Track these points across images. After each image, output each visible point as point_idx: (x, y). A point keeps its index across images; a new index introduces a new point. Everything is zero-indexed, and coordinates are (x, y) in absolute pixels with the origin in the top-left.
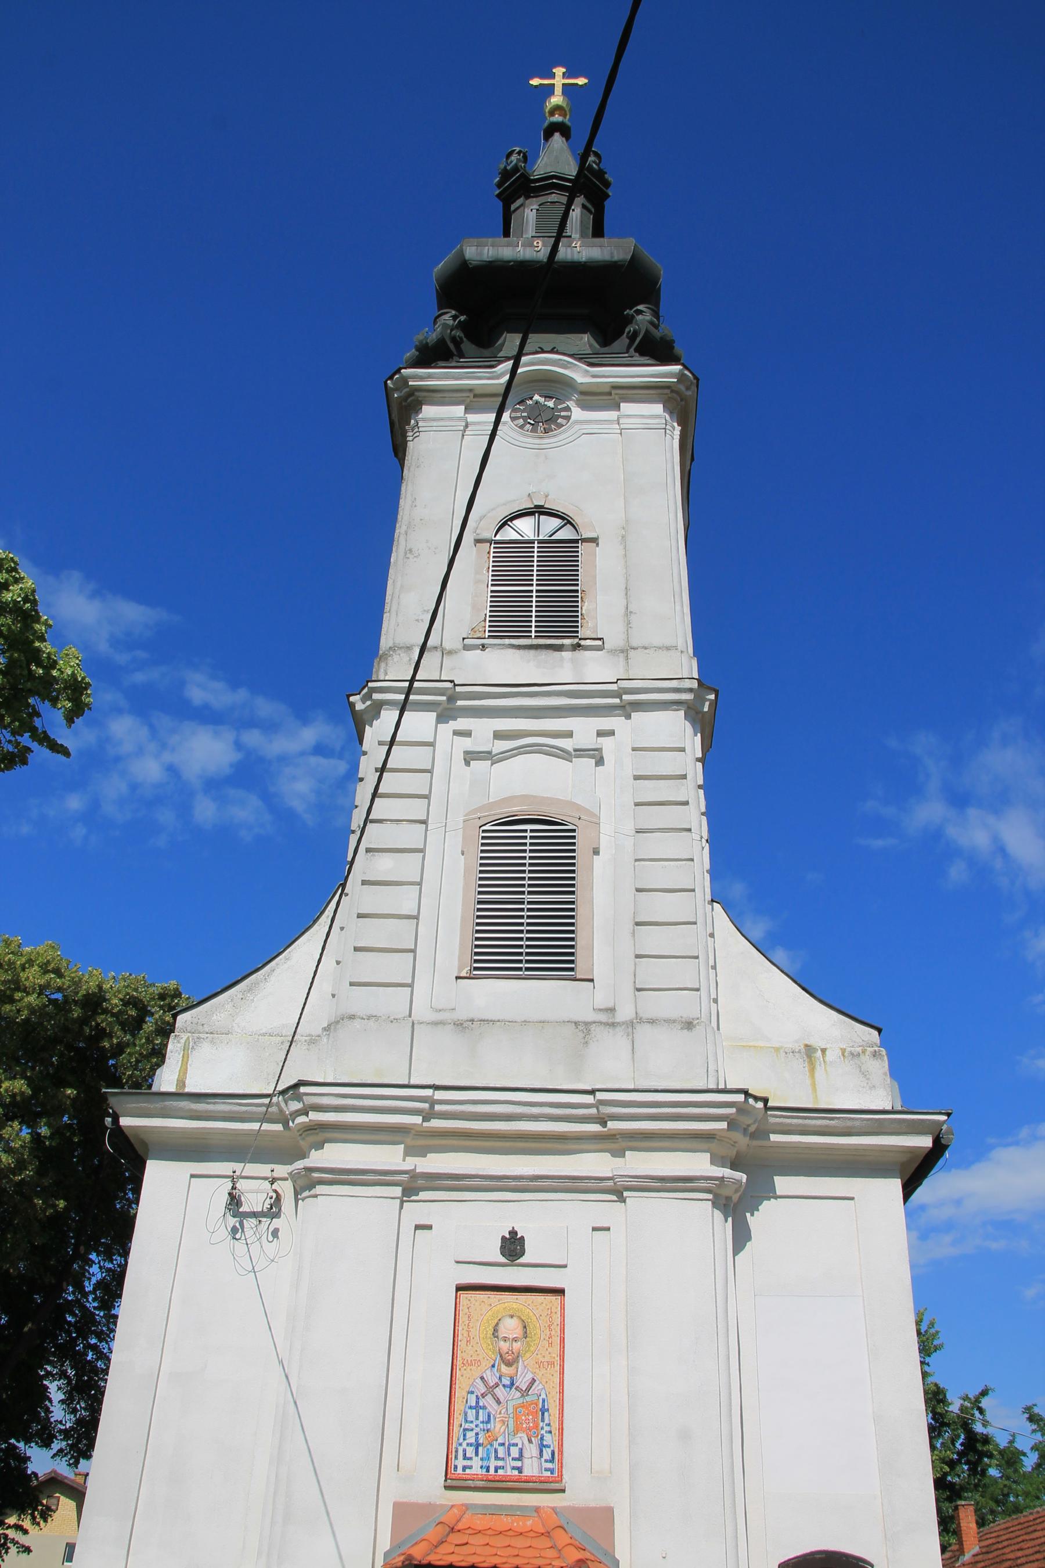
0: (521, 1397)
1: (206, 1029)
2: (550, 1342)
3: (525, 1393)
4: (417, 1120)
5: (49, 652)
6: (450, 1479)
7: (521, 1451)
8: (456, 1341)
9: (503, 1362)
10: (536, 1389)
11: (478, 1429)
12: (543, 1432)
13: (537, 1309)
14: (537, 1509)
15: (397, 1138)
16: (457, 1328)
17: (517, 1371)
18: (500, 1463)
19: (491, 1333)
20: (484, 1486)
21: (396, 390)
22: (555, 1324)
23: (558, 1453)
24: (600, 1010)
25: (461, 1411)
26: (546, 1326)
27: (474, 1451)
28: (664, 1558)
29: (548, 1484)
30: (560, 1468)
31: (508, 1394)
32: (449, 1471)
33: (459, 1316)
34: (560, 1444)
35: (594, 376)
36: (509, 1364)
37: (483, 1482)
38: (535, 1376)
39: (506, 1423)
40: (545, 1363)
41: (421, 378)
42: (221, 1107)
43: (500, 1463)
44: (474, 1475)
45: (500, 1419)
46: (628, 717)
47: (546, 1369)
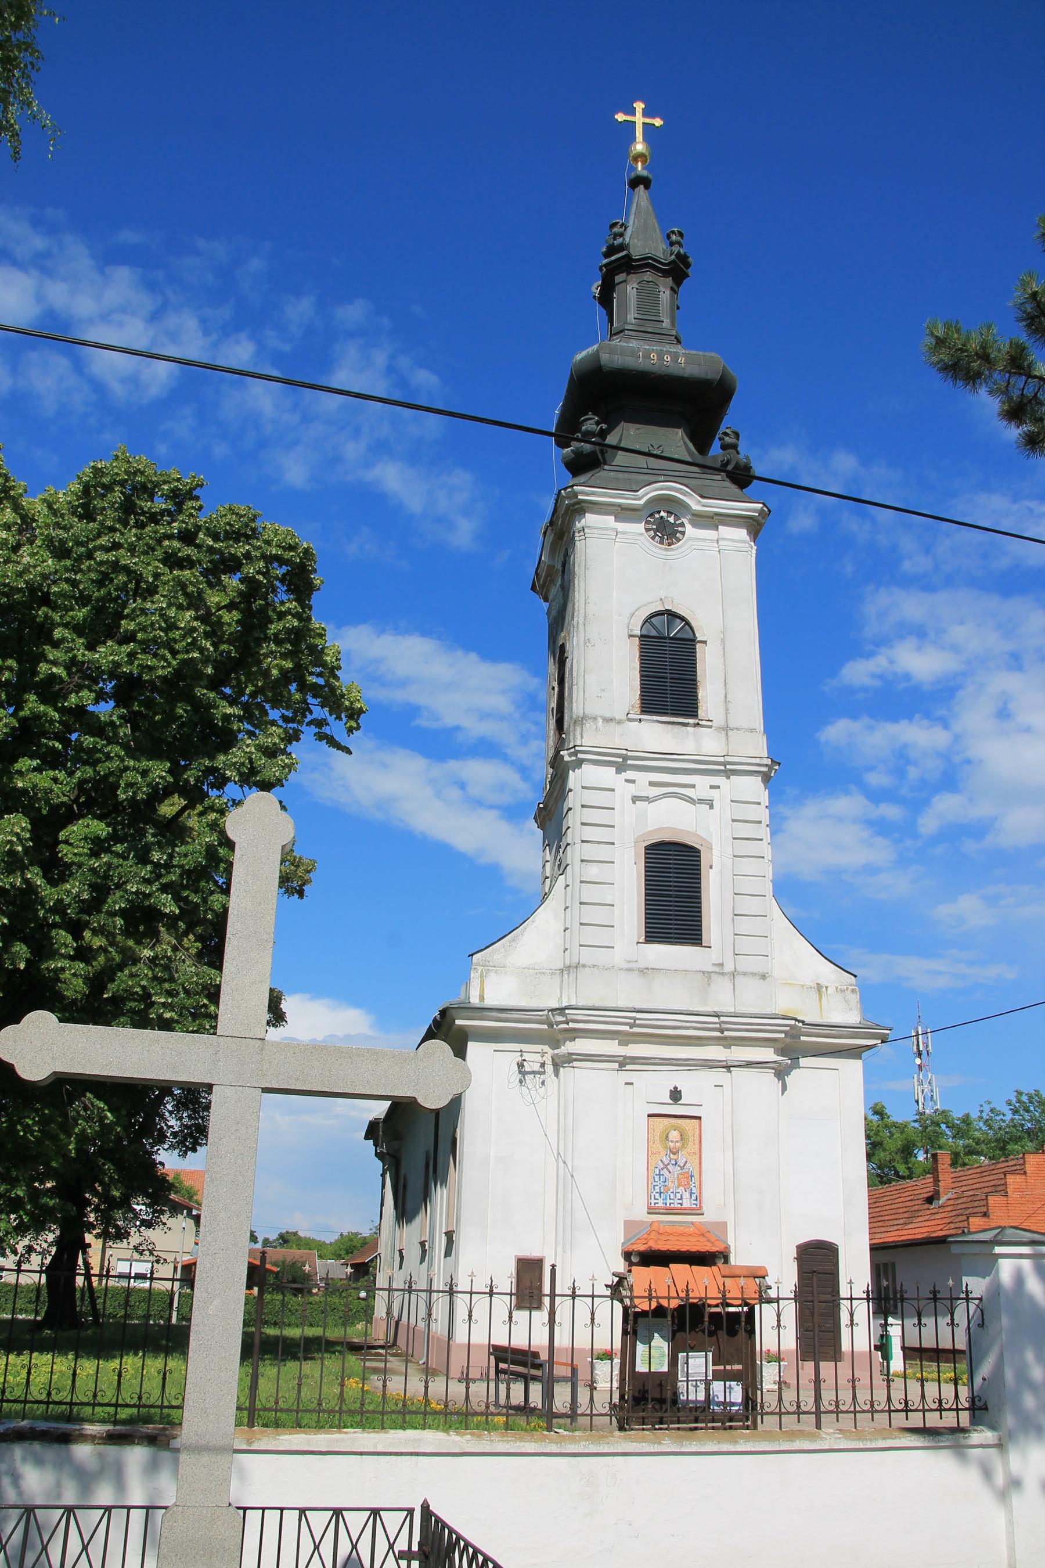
1: (491, 964)
3: (682, 1168)
4: (627, 1028)
5: (202, 589)
7: (681, 1196)
14: (692, 1223)
15: (615, 1037)
18: (656, 1201)
21: (567, 498)
24: (716, 964)
35: (704, 506)
36: (674, 1154)
41: (587, 494)
42: (515, 1015)
43: (656, 1201)
46: (728, 778)
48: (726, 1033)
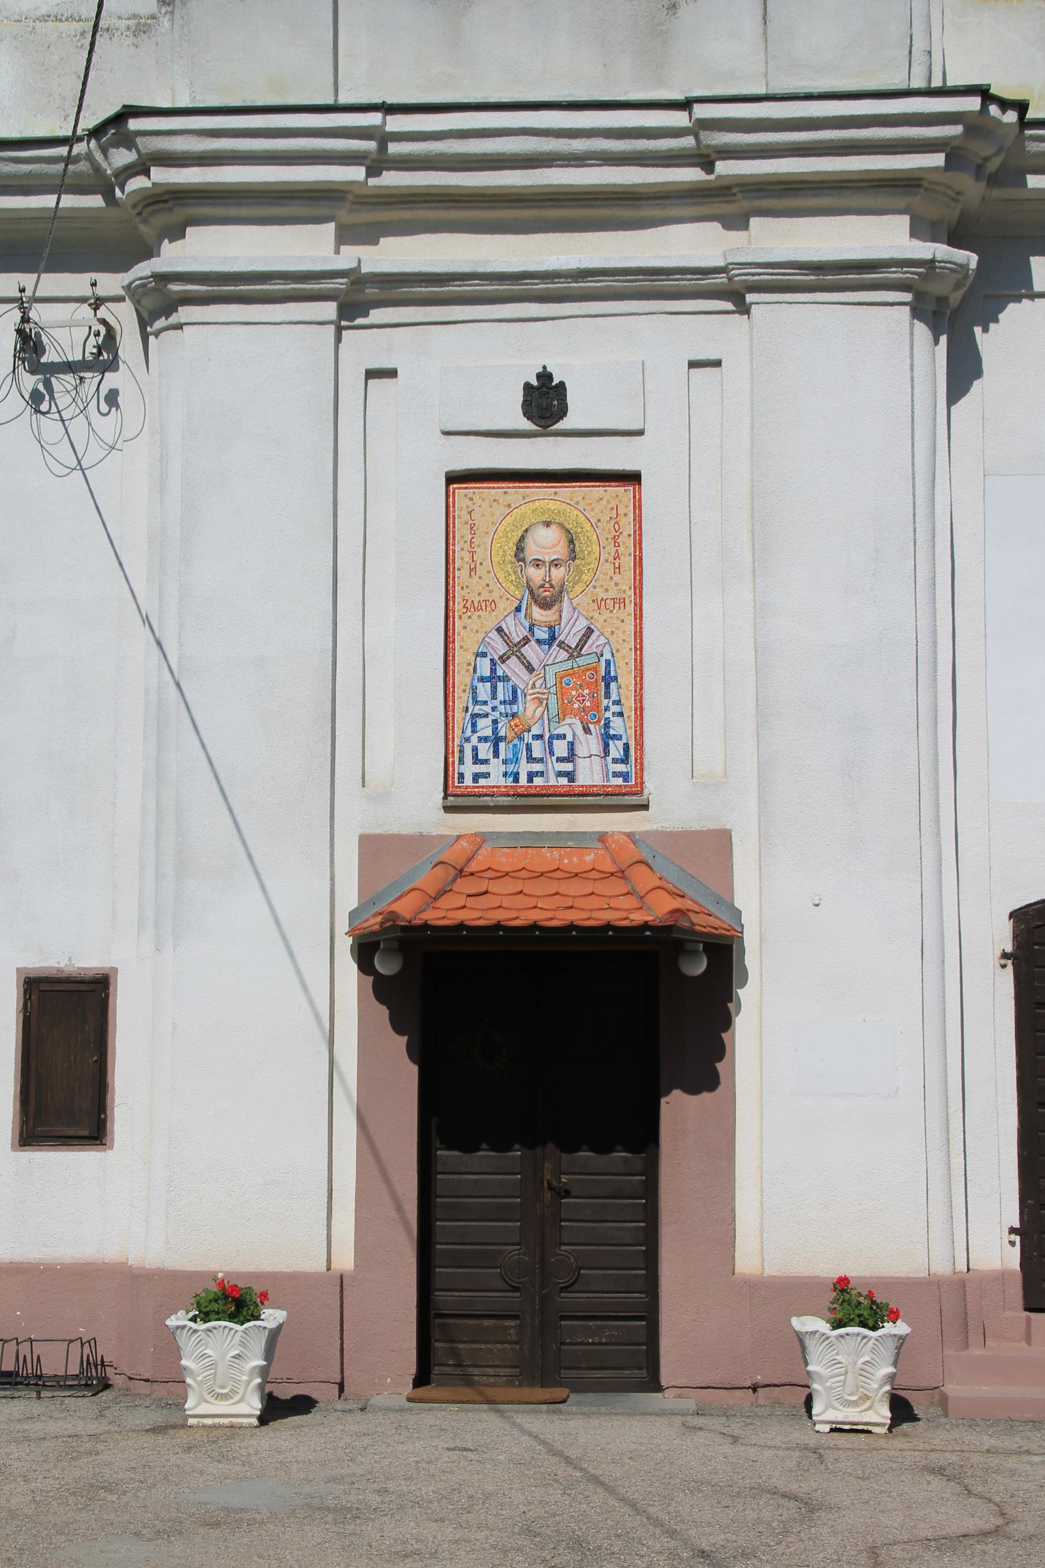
3: (575, 652)
4: (357, 173)
7: (571, 746)
14: (602, 837)
18: (537, 767)
36: (546, 605)
43: (537, 767)
48: (724, 168)
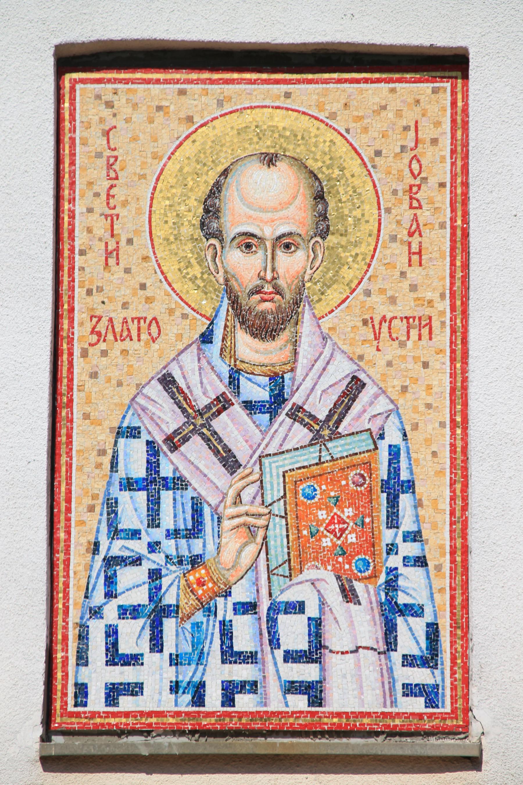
0: (311, 445)
2: (415, 248)
6: (177, 545)
8: (66, 253)
9: (242, 323)
10: (367, 416)
11: (159, 558)
12: (394, 561)
13: (365, 130)
16: (66, 206)
17: (295, 353)
19: (197, 222)
20: (187, 751)
22: (433, 181)
23: (452, 634)
25: (95, 497)
26: (400, 188)
27: (147, 634)
28: (159, 108)
29: (418, 740)
30: (459, 684)
31: (264, 433)
32: (58, 704)
33: (72, 163)
34: (458, 601)
37: (184, 740)
38: (361, 369)
39: (261, 533)
40: (395, 322)
44: (150, 714)
45: (237, 521)
47: (403, 345)
